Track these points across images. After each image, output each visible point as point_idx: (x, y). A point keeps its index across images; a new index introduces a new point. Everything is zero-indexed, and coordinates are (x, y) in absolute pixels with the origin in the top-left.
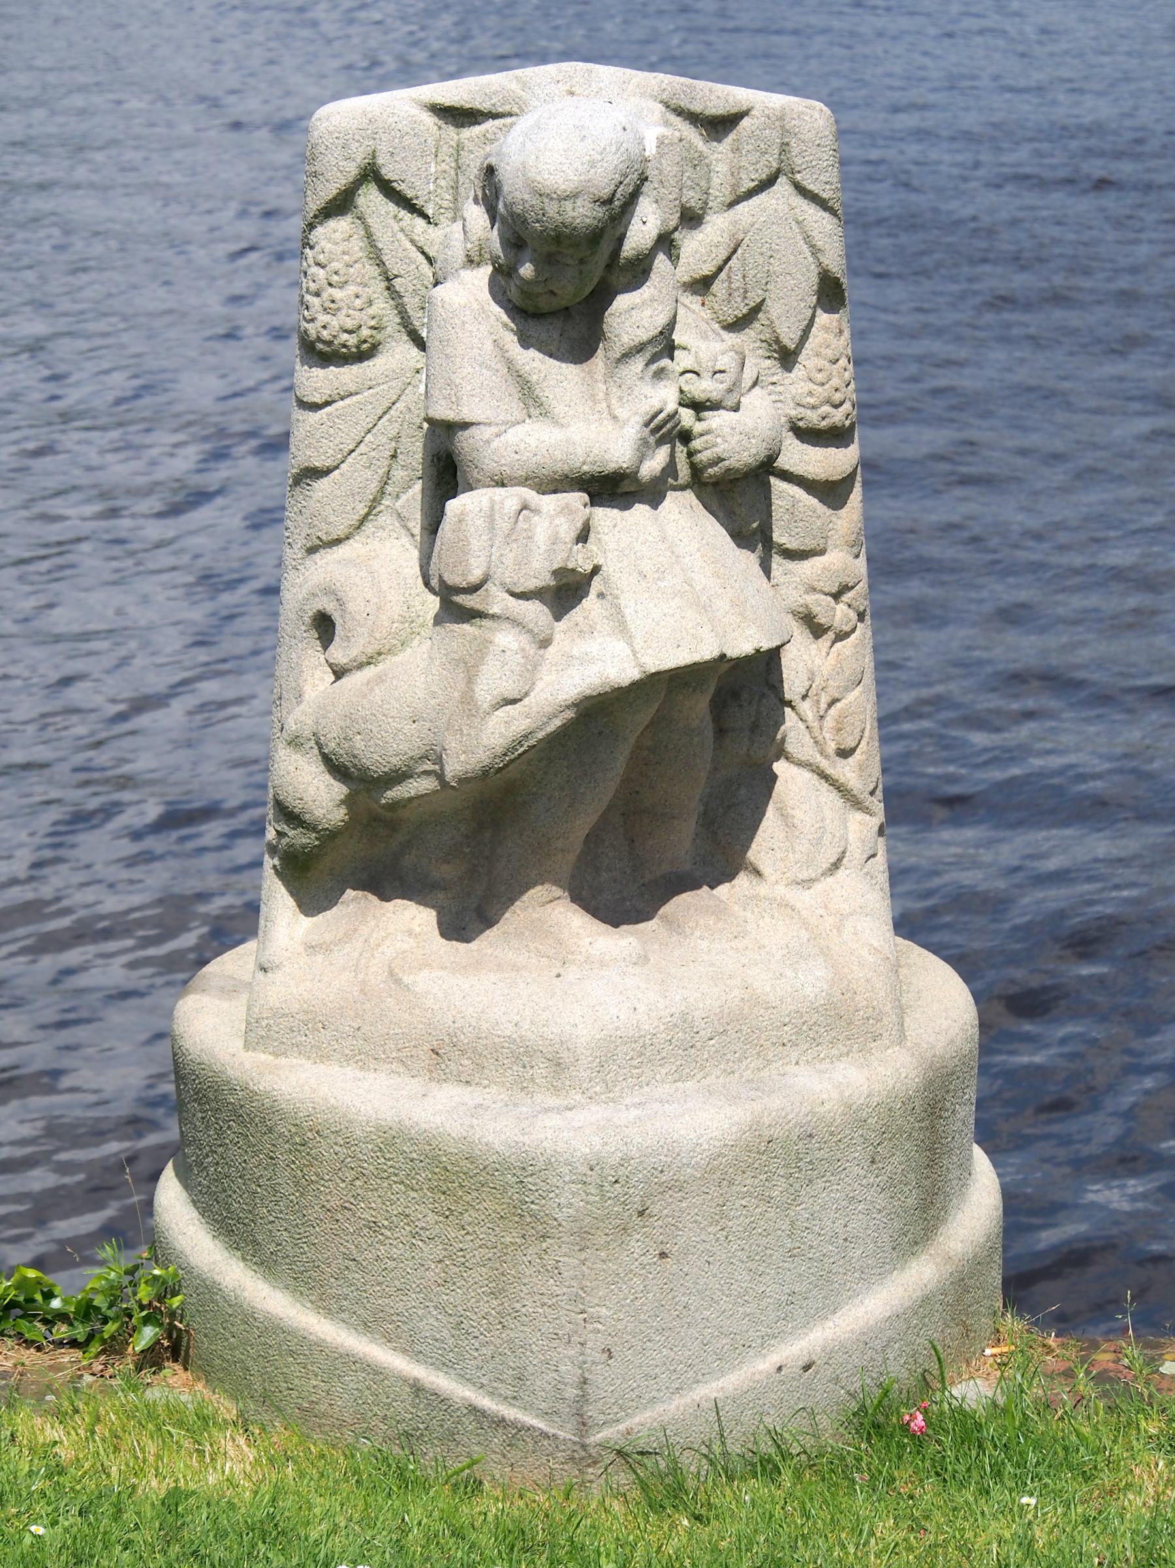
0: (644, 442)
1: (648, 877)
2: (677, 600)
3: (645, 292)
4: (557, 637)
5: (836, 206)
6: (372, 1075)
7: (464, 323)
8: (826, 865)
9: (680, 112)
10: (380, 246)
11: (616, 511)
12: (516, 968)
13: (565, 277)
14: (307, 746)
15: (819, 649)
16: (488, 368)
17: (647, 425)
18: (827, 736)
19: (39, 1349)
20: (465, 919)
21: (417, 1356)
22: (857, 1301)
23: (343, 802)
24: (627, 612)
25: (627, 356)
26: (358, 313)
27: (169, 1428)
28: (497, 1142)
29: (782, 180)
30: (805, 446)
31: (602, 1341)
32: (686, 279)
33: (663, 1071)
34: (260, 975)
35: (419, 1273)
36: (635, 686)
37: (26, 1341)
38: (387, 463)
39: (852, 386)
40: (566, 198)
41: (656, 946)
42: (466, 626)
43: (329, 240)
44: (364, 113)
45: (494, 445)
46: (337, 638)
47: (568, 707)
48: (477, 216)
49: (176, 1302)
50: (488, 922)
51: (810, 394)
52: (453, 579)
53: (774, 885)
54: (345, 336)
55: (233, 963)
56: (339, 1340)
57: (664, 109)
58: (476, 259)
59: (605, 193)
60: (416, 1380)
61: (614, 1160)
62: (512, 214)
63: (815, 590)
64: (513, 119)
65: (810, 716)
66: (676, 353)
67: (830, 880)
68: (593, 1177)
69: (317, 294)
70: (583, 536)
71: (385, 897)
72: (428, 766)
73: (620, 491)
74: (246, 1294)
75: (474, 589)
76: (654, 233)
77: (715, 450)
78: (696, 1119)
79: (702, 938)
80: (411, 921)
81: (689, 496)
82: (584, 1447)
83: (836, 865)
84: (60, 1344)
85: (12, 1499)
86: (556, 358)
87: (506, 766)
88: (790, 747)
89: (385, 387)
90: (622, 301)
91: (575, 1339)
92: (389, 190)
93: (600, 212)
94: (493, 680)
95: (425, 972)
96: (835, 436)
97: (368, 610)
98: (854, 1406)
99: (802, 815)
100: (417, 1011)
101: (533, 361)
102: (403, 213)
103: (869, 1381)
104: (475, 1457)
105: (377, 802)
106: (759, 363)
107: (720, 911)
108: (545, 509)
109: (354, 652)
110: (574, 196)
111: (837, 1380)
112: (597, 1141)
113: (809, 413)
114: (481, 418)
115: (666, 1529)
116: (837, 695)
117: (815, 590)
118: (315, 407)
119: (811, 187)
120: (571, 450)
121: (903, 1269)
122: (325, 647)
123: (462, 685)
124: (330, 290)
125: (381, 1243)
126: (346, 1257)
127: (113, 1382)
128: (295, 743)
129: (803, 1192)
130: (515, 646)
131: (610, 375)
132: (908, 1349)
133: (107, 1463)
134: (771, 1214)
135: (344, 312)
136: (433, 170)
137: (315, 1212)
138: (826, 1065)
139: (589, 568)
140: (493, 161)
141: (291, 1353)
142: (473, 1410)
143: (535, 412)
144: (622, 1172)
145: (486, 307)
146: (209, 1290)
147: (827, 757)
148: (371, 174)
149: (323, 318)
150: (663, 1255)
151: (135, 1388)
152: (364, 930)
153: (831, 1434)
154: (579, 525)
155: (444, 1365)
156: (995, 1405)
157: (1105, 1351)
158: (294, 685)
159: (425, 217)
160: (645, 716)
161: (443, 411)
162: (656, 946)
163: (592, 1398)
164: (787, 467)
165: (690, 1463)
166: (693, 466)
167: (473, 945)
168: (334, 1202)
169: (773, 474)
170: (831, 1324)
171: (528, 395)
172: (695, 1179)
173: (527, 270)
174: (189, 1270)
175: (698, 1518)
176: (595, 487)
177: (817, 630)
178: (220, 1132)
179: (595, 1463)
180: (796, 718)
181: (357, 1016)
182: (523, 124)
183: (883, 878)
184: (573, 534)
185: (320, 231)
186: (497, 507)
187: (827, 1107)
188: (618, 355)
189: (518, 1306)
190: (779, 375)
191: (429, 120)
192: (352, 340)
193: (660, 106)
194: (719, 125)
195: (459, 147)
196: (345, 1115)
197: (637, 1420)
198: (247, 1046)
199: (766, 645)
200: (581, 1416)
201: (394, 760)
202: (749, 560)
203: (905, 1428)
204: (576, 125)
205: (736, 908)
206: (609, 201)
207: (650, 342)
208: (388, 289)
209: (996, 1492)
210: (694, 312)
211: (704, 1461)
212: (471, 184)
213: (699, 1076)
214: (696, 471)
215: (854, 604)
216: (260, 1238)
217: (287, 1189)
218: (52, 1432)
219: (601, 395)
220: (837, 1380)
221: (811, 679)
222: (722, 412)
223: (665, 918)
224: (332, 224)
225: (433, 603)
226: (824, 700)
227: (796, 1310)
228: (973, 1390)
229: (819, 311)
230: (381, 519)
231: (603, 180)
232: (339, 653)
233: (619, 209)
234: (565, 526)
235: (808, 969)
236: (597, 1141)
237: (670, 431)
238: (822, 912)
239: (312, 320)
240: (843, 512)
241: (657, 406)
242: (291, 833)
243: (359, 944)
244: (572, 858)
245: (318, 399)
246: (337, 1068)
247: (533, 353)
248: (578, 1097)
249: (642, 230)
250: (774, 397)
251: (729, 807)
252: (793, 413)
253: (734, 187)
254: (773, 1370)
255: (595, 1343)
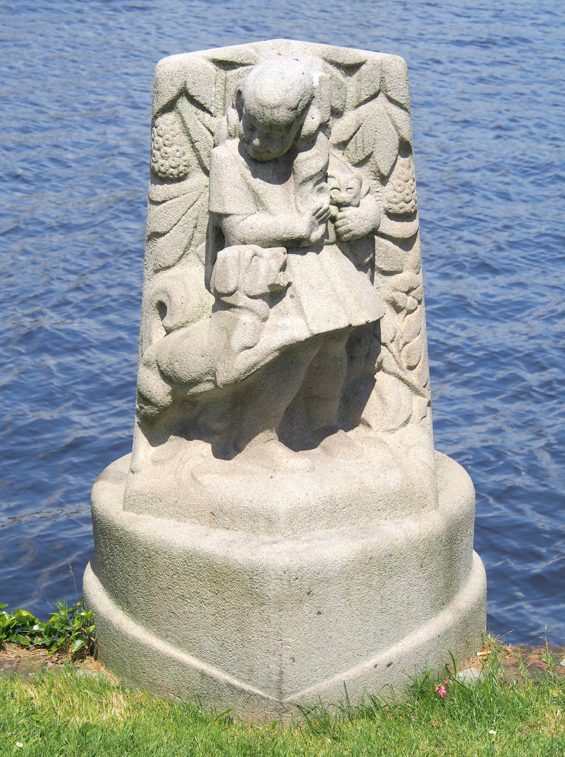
0: (313, 223)
1: (316, 428)
2: (328, 299)
3: (314, 151)
4: (271, 316)
5: (407, 107)
6: (183, 524)
7: (226, 166)
8: (402, 422)
9: (332, 63)
10: (188, 127)
11: (299, 256)
12: (252, 473)
13: (274, 146)
14: (153, 366)
15: (399, 318)
16: (238, 188)
17: (314, 215)
18: (403, 360)
19: (28, 649)
20: (227, 449)
21: (203, 659)
22: (413, 633)
23: (169, 393)
24: (304, 305)
25: (305, 182)
26: (178, 159)
27: (86, 691)
28: (240, 559)
29: (381, 94)
30: (392, 221)
31: (290, 654)
32: (335, 142)
33: (321, 524)
34: (131, 474)
35: (204, 620)
36: (307, 340)
37: (22, 645)
38: (192, 230)
39: (415, 192)
40: (275, 107)
41: (319, 462)
42: (227, 312)
43: (164, 124)
44: (181, 64)
45: (241, 224)
46: (167, 314)
47: (275, 351)
48: (233, 114)
49: (92, 628)
50: (238, 450)
51: (395, 197)
52: (220, 289)
53: (376, 432)
54: (172, 170)
55: (120, 465)
56: (167, 650)
57: (323, 62)
58: (233, 134)
59: (294, 105)
60: (202, 670)
61: (295, 568)
62: (249, 115)
63: (397, 290)
64: (252, 66)
65: (395, 350)
66: (329, 179)
67: (403, 429)
68: (285, 576)
69: (159, 150)
70: (283, 268)
71: (189, 438)
72: (210, 378)
73: (301, 246)
74: (124, 627)
75: (231, 294)
76: (318, 123)
77: (347, 226)
78: (335, 548)
79: (341, 458)
80: (202, 448)
81: (335, 247)
82: (281, 704)
83: (406, 422)
84: (38, 647)
85: (9, 728)
86: (271, 183)
87: (246, 378)
88: (385, 365)
89: (191, 194)
90: (302, 156)
91: (277, 653)
92: (192, 100)
93: (291, 114)
94: (240, 338)
95: (208, 475)
96: (407, 217)
97: (182, 301)
98: (411, 683)
99: (390, 398)
100: (204, 494)
101: (259, 184)
102: (199, 111)
103: (419, 671)
104: (231, 707)
105: (186, 394)
106: (369, 182)
107: (350, 444)
108: (265, 255)
109: (175, 322)
110: (278, 107)
111: (403, 671)
112: (287, 559)
113: (394, 206)
114: (235, 212)
115: (319, 744)
116: (408, 340)
117: (397, 290)
118: (158, 203)
119: (395, 98)
120: (277, 227)
121: (436, 616)
122: (162, 318)
123: (225, 340)
124: (165, 148)
125: (186, 605)
126: (170, 611)
127: (61, 666)
128: (147, 364)
129: (387, 582)
130: (250, 321)
131: (296, 191)
132: (438, 655)
133: (56, 708)
134: (372, 593)
135: (171, 158)
136: (214, 91)
137: (155, 590)
138: (399, 520)
139: (286, 284)
140: (241, 88)
141: (145, 656)
142: (229, 685)
143: (261, 208)
144: (299, 574)
145: (237, 158)
146: (106, 624)
147: (402, 370)
148: (184, 92)
149: (161, 161)
150: (319, 613)
151: (70, 669)
152: (180, 454)
153: (401, 697)
154: (281, 263)
155: (215, 664)
156: (479, 681)
157: (535, 654)
158: (148, 335)
159: (210, 113)
160: (314, 353)
161: (217, 208)
162: (319, 462)
163: (285, 681)
164: (384, 232)
165: (333, 712)
166: (337, 233)
167: (232, 462)
168: (164, 585)
169: (377, 235)
170: (401, 644)
171: (258, 201)
172: (335, 577)
173: (256, 142)
174: (97, 613)
175: (335, 739)
176: (290, 244)
177: (398, 309)
178: (112, 549)
179: (287, 711)
180: (388, 351)
181: (176, 495)
182: (256, 70)
183: (430, 427)
184: (278, 268)
185: (160, 120)
186: (242, 255)
187: (399, 541)
188: (300, 182)
189: (250, 637)
190: (380, 188)
191: (212, 67)
192: (175, 172)
193: (322, 60)
194: (351, 69)
195: (226, 80)
196: (169, 545)
197: (307, 691)
198: (124, 509)
199: (371, 320)
200: (280, 689)
201: (193, 375)
202: (364, 277)
203: (436, 694)
204: (282, 71)
205: (358, 443)
206: (296, 108)
207: (316, 175)
208: (192, 147)
209: (478, 725)
210: (338, 159)
211: (339, 710)
212: (231, 99)
213: (338, 526)
214: (339, 236)
215: (416, 296)
216: (130, 600)
217: (142, 578)
218: (32, 692)
219: (293, 200)
220: (403, 671)
221: (395, 333)
222: (351, 207)
223: (324, 448)
224: (166, 116)
225: (212, 300)
226: (401, 342)
227: (383, 638)
228: (469, 674)
229: (399, 157)
230: (190, 257)
231: (292, 99)
232: (169, 322)
233: (301, 112)
234: (274, 264)
235: (397, 467)
236: (287, 559)
237: (325, 218)
238: (399, 445)
239: (156, 162)
240: (410, 252)
241: (319, 206)
242: (146, 407)
243: (177, 460)
244: (279, 420)
245: (159, 199)
246: (166, 520)
247: (258, 180)
248: (280, 537)
249: (311, 122)
250: (377, 198)
251: (355, 394)
252: (387, 206)
253: (358, 98)
254: (372, 667)
255: (287, 655)
